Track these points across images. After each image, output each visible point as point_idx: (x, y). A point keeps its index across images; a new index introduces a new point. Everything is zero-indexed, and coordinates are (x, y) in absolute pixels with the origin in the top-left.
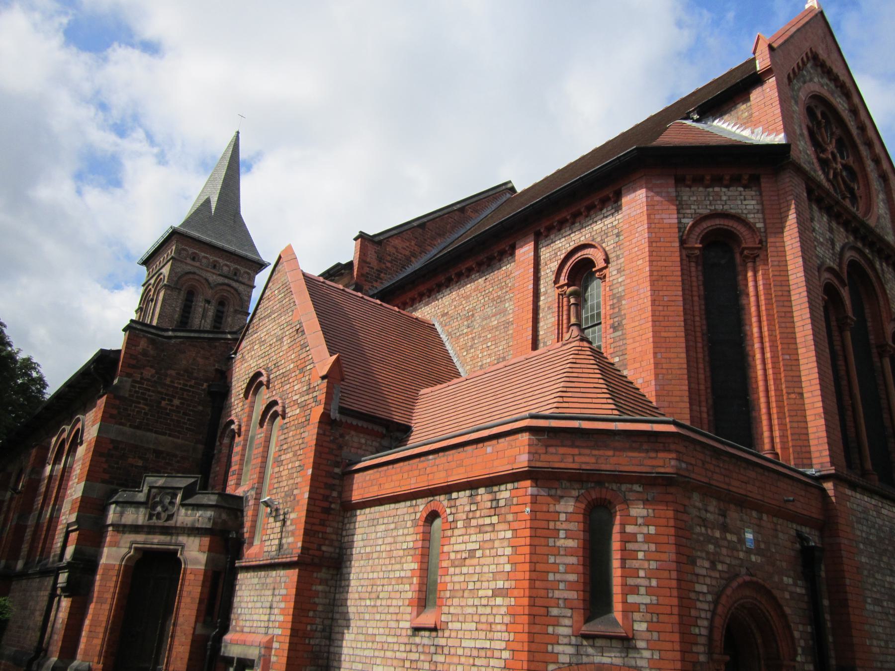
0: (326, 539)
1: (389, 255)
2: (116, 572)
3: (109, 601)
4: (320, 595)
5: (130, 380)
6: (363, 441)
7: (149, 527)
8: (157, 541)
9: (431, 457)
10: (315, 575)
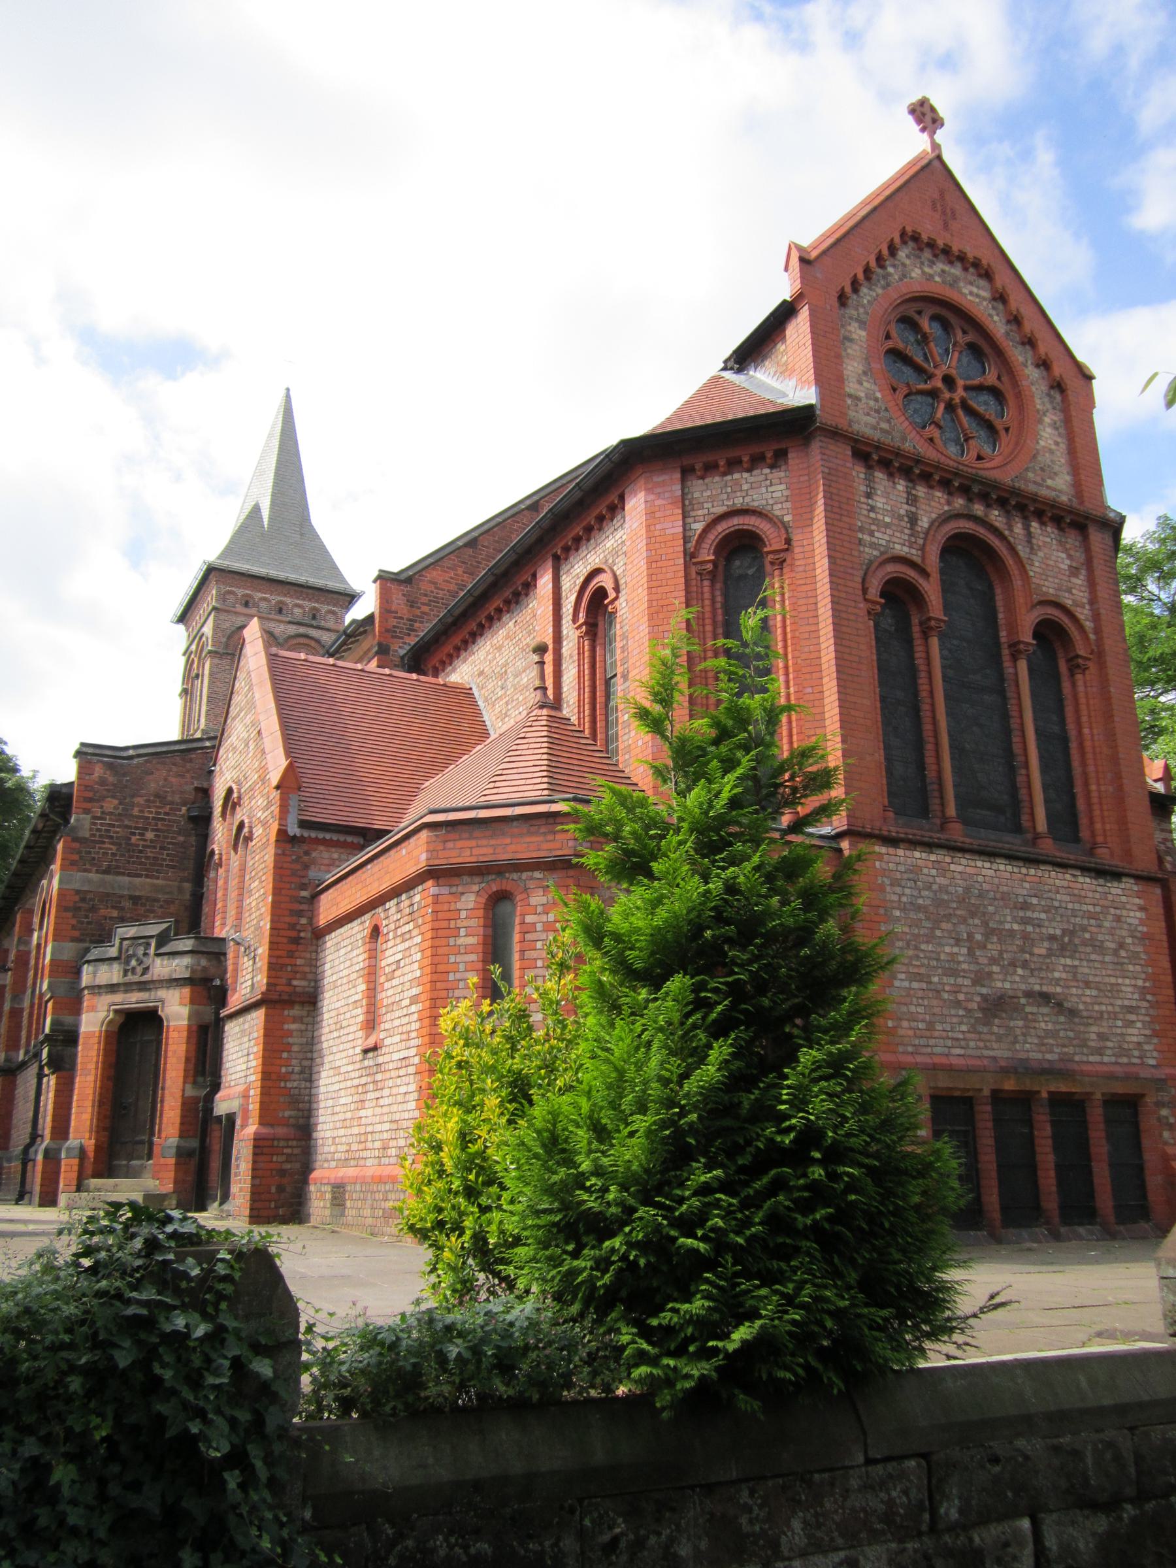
0: (296, 972)
1: (426, 595)
2: (96, 1040)
3: (93, 1072)
4: (295, 1034)
5: (89, 817)
6: (336, 856)
7: (125, 984)
8: (135, 1000)
9: (369, 866)
10: (286, 1012)
